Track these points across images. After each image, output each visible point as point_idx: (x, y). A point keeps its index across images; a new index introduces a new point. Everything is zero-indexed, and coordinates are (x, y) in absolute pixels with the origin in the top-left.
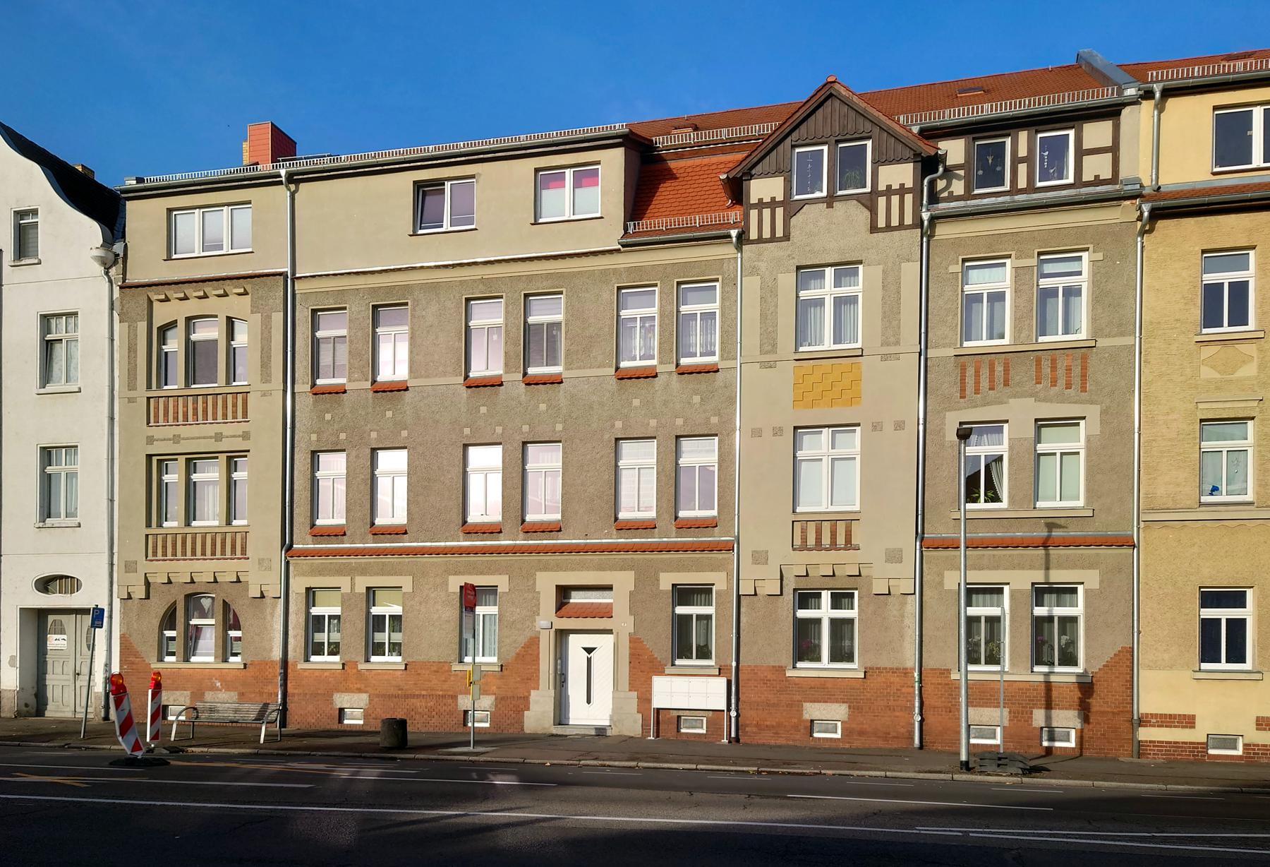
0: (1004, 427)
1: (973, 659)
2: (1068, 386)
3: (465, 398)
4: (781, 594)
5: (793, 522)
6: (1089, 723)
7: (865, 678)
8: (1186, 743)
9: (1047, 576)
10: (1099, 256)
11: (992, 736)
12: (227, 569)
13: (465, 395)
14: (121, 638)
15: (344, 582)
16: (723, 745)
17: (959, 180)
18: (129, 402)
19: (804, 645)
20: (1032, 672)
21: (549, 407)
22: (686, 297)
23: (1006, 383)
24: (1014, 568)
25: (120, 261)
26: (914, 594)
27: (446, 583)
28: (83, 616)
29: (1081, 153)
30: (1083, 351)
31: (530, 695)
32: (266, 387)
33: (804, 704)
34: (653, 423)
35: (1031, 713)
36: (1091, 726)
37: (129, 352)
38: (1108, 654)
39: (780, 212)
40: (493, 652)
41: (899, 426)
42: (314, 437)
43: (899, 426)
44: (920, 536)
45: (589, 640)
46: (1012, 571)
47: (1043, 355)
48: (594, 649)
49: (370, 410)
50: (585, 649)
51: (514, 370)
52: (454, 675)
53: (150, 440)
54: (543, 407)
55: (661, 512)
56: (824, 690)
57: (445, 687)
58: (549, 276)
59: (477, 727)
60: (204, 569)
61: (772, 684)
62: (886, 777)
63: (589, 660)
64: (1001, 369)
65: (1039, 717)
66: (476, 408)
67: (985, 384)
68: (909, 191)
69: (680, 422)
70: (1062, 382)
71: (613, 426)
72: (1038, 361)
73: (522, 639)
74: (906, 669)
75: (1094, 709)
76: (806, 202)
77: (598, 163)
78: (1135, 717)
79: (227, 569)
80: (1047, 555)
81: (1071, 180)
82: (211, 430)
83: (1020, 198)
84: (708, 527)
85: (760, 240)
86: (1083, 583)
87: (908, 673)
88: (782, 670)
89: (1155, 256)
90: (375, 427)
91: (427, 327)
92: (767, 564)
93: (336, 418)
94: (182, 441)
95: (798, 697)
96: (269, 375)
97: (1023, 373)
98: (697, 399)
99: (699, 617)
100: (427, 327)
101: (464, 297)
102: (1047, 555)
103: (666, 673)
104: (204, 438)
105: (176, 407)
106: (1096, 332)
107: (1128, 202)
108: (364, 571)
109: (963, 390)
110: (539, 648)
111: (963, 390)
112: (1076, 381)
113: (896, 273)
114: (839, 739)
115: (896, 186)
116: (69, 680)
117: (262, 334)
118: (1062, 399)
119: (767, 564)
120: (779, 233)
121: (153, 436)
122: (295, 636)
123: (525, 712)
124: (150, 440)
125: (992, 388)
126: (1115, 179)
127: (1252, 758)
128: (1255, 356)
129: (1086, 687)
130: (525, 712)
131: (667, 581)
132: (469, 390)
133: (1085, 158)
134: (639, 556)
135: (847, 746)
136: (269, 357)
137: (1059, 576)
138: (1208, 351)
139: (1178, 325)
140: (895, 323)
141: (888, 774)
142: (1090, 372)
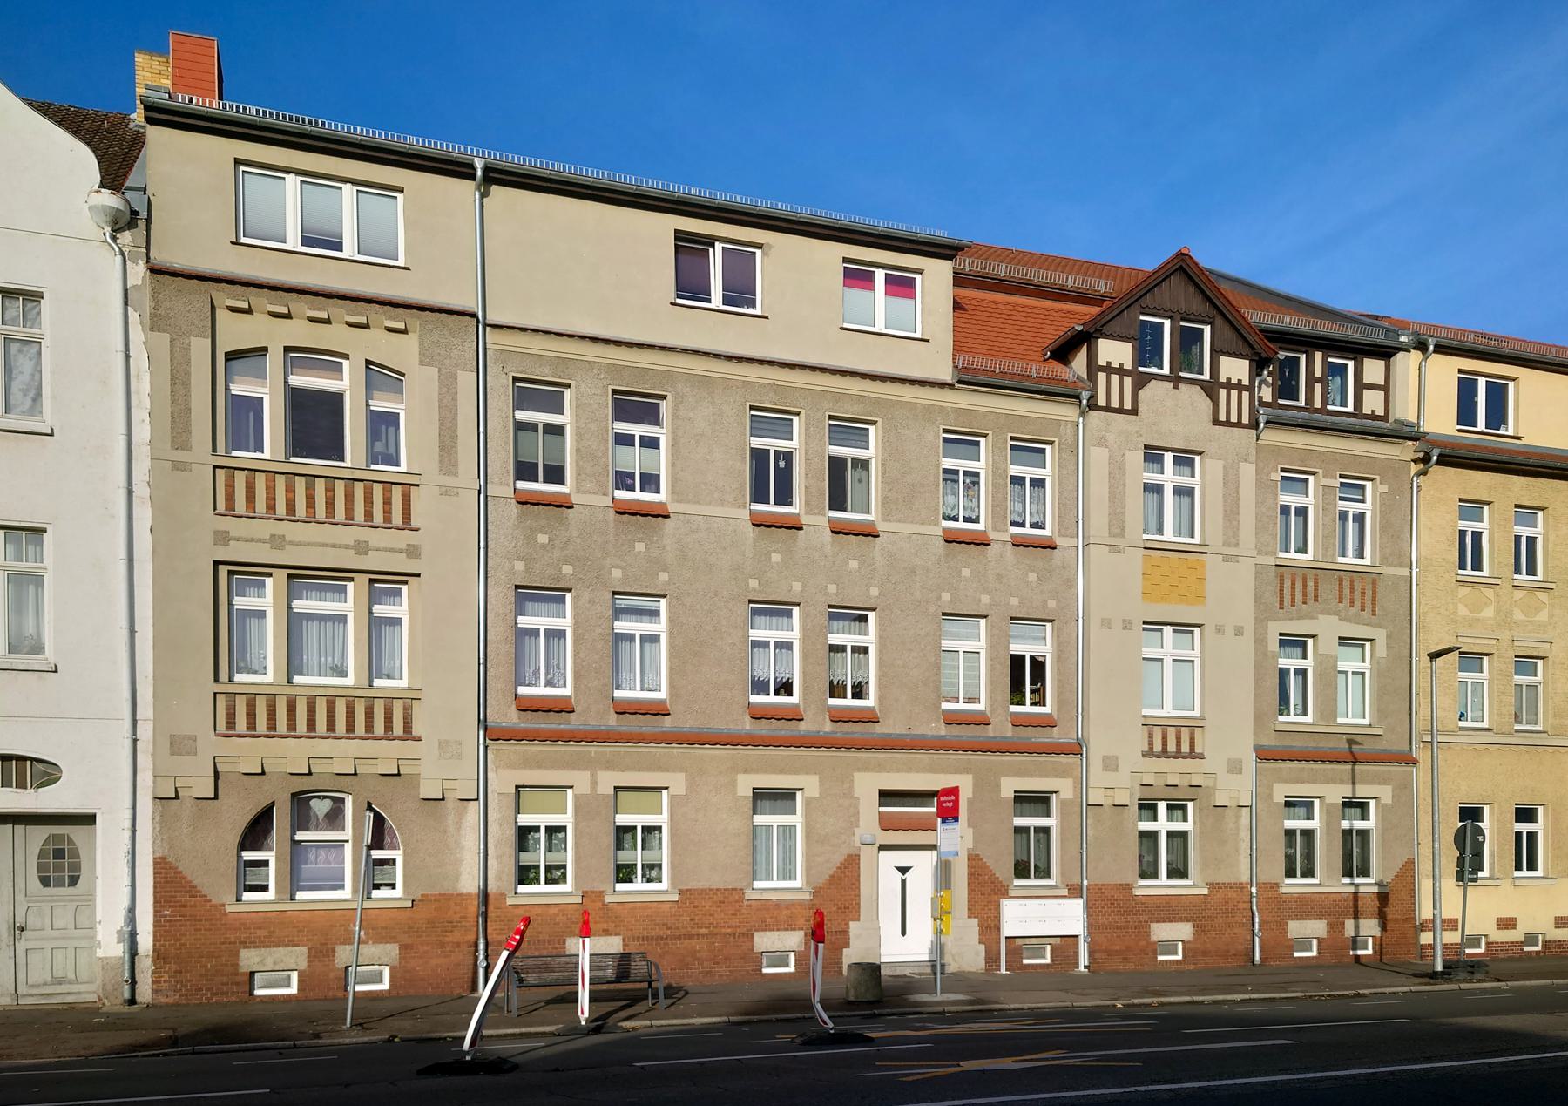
0: (794, 612)
1: (1290, 873)
2: (1363, 610)
3: (751, 540)
4: (216, 797)
5: (215, 694)
6: (1386, 931)
7: (412, 907)
8: (1452, 944)
9: (1354, 790)
10: (1384, 488)
11: (286, 984)
12: (382, 755)
13: (752, 535)
14: (155, 863)
15: (580, 780)
16: (1082, 975)
17: (1269, 387)
19: (1299, 856)
20: (516, 893)
21: (861, 565)
22: (10, 349)
23: (1316, 600)
24: (1328, 783)
25: (142, 224)
26: (477, 800)
27: (734, 784)
28: (27, 827)
29: (1360, 386)
30: (1373, 576)
31: (848, 928)
32: (449, 481)
33: (1152, 924)
34: (985, 599)
35: (1344, 924)
36: (1388, 932)
38: (1398, 865)
39: (1128, 381)
40: (788, 875)
41: (1239, 631)
42: (520, 566)
43: (1239, 631)
44: (483, 723)
45: (903, 858)
46: (907, 774)
47: (1346, 577)
48: (909, 868)
49: (611, 537)
50: (898, 868)
51: (816, 511)
52: (747, 906)
53: (222, 538)
54: (854, 564)
55: (995, 706)
56: (1169, 909)
57: (735, 922)
58: (861, 399)
59: (358, 992)
60: (337, 755)
61: (1119, 904)
62: (1411, 991)
63: (903, 882)
64: (1312, 584)
65: (1349, 925)
66: (765, 554)
67: (1299, 597)
68: (1246, 388)
69: (1014, 601)
70: (1358, 604)
71: (939, 598)
72: (1341, 580)
73: (838, 858)
74: (1242, 884)
75: (1389, 917)
76: (1154, 376)
77: (920, 272)
78: (1418, 924)
79: (382, 755)
80: (1353, 770)
81: (1350, 408)
84: (549, 711)
85: (1108, 409)
86: (572, 787)
87: (1243, 888)
88: (1128, 888)
89: (1428, 497)
90: (619, 562)
91: (697, 435)
92: (1117, 771)
93: (557, 543)
94: (287, 546)
95: (1143, 918)
96: (455, 464)
97: (1328, 590)
98: (1033, 577)
99: (1037, 830)
100: (695, 436)
101: (610, 388)
102: (1353, 770)
103: (1010, 895)
104: (334, 546)
105: (271, 489)
106: (1385, 561)
107: (1410, 443)
108: (610, 765)
109: (1282, 601)
110: (859, 868)
111: (1282, 601)
112: (1368, 604)
113: (1236, 472)
114: (1048, 965)
115: (1234, 381)
117: (440, 401)
118: (1357, 621)
119: (1117, 771)
122: (498, 858)
123: (844, 950)
125: (1304, 603)
126: (1385, 418)
127: (1495, 954)
128: (1493, 599)
129: (1383, 897)
130: (844, 950)
131: (1009, 787)
132: (757, 529)
134: (979, 757)
135: (1192, 967)
136: (454, 437)
137: (1362, 791)
138: (1519, 594)
139: (1444, 564)
140: (1235, 523)
141: (654, 1022)
142: (1379, 596)
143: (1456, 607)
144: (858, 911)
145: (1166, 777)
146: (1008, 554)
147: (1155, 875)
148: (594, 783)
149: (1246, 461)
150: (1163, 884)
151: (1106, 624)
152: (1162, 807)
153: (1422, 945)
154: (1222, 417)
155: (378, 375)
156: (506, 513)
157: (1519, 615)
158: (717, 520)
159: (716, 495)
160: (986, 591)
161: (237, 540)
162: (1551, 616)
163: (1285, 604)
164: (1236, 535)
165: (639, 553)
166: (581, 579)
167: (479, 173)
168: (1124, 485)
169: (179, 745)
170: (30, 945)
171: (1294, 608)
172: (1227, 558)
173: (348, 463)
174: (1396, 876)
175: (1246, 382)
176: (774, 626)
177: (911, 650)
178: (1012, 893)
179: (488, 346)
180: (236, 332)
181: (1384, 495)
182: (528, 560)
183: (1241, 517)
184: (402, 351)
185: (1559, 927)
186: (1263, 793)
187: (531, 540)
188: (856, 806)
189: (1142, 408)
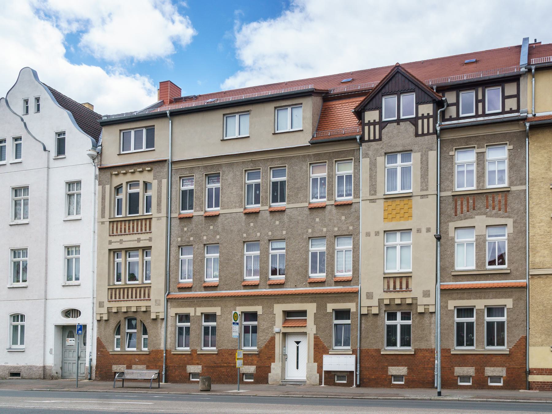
14: (97, 339)
18: (102, 224)
23: (474, 209)
37: (102, 200)
39: (377, 127)
51: (265, 204)
53: (150, 240)
54: (277, 223)
56: (397, 360)
63: (298, 347)
67: (465, 209)
68: (431, 117)
69: (336, 229)
70: (497, 208)
71: (307, 231)
82: (135, 237)
85: (369, 141)
88: (379, 351)
98: (343, 218)
106: (511, 183)
109: (456, 212)
111: (456, 212)
112: (503, 207)
116: (75, 360)
118: (497, 216)
120: (377, 137)
121: (140, 238)
124: (110, 242)
125: (468, 211)
136: (161, 201)
144: (274, 359)
145: (383, 301)
146: (333, 210)
147: (395, 345)
148: (195, 312)
149: (431, 150)
150: (399, 349)
151: (368, 234)
152: (399, 315)
153: (529, 382)
154: (420, 132)
155: (146, 185)
156: (175, 222)
158: (233, 214)
159: (234, 204)
161: (142, 240)
163: (458, 213)
164: (427, 185)
165: (211, 229)
166: (195, 241)
167: (168, 115)
168: (376, 172)
169: (101, 305)
170: (81, 362)
171: (462, 215)
172: (422, 196)
174: (515, 345)
175: (431, 114)
176: (257, 250)
177: (297, 254)
178: (330, 353)
179: (173, 169)
180: (117, 181)
181: (511, 151)
182: (181, 237)
183: (429, 177)
184: (147, 177)
186: (444, 307)
187: (182, 230)
188: (275, 318)
189: (384, 137)
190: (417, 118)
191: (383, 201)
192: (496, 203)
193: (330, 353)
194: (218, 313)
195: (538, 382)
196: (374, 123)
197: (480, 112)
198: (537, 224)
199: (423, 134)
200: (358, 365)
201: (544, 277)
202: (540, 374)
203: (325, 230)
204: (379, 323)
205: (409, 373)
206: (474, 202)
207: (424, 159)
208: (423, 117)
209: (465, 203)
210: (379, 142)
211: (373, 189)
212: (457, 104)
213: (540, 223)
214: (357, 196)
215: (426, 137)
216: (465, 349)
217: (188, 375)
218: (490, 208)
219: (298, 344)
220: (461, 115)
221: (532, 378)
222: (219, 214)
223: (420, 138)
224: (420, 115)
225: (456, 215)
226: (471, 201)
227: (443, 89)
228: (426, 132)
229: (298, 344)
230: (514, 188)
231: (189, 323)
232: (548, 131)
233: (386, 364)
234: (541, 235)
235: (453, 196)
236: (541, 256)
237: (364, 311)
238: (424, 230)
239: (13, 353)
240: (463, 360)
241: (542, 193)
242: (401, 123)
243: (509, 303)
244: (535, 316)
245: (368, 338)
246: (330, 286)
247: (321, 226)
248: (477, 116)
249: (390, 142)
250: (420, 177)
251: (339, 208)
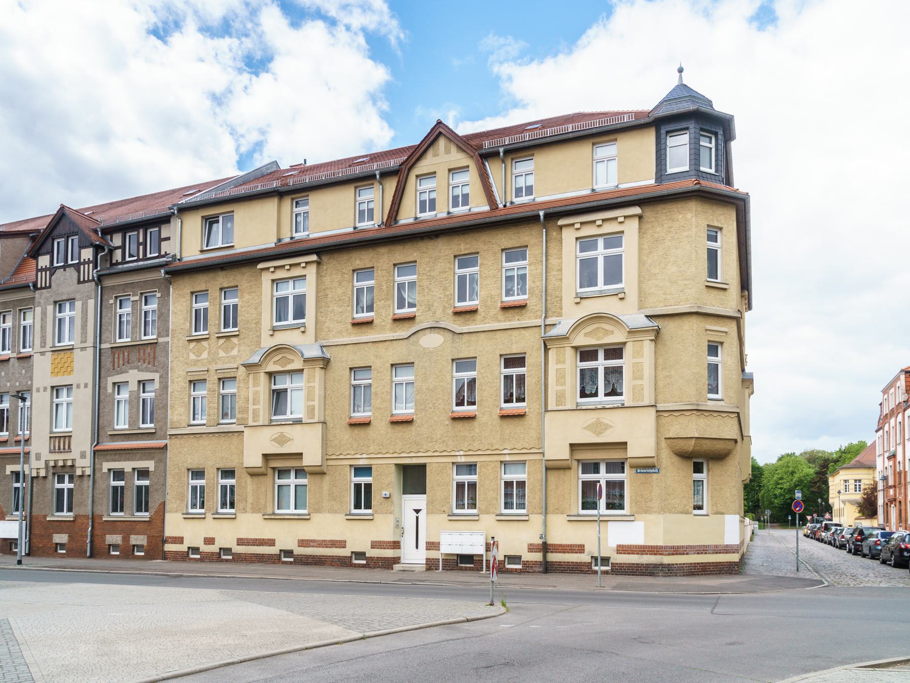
2: (149, 364)
41: (86, 386)
50: (414, 510)
56: (60, 526)
63: (417, 518)
67: (121, 362)
68: (91, 262)
69: (17, 384)
83: (141, 263)
85: (42, 288)
106: (159, 335)
109: (114, 366)
112: (152, 360)
115: (44, 267)
120: (48, 285)
125: (123, 365)
133: (162, 243)
143: (188, 354)
154: (82, 280)
157: (222, 354)
160: (9, 381)
162: (239, 351)
173: (719, 281)
178: (6, 519)
185: (239, 545)
189: (53, 284)
190: (79, 264)
191: (51, 353)
192: (147, 355)
193: (6, 519)
194: (152, 469)
195: (172, 551)
196: (46, 269)
197: (141, 257)
198: (176, 380)
199: (84, 282)
200: (28, 531)
201: (180, 437)
202: (175, 543)
203: (8, 384)
204: (48, 486)
205: (69, 541)
206: (128, 355)
207: (84, 308)
208: (85, 263)
209: (121, 355)
210: (49, 290)
211: (43, 343)
212: (123, 247)
213: (178, 378)
214: (164, 331)
215: (86, 284)
216: (118, 515)
217: (131, 547)
218: (142, 361)
219: (417, 513)
220: (149, 256)
221: (169, 547)
222: (9, 358)
223: (81, 285)
224: (39, 268)
225: (114, 369)
226: (126, 354)
227: (109, 231)
228: (86, 279)
229: (417, 513)
230: (161, 340)
231: (124, 482)
232: (187, 277)
233: (52, 531)
234: (178, 391)
235: (112, 348)
236: (178, 414)
237: (34, 474)
238: (82, 386)
239: (221, 520)
240: (113, 526)
241: (181, 345)
242: (67, 269)
243: (150, 465)
244: (172, 480)
245: (38, 502)
246: (11, 446)
247: (6, 381)
248: (138, 260)
249: (58, 290)
250: (80, 327)
251: (21, 361)
